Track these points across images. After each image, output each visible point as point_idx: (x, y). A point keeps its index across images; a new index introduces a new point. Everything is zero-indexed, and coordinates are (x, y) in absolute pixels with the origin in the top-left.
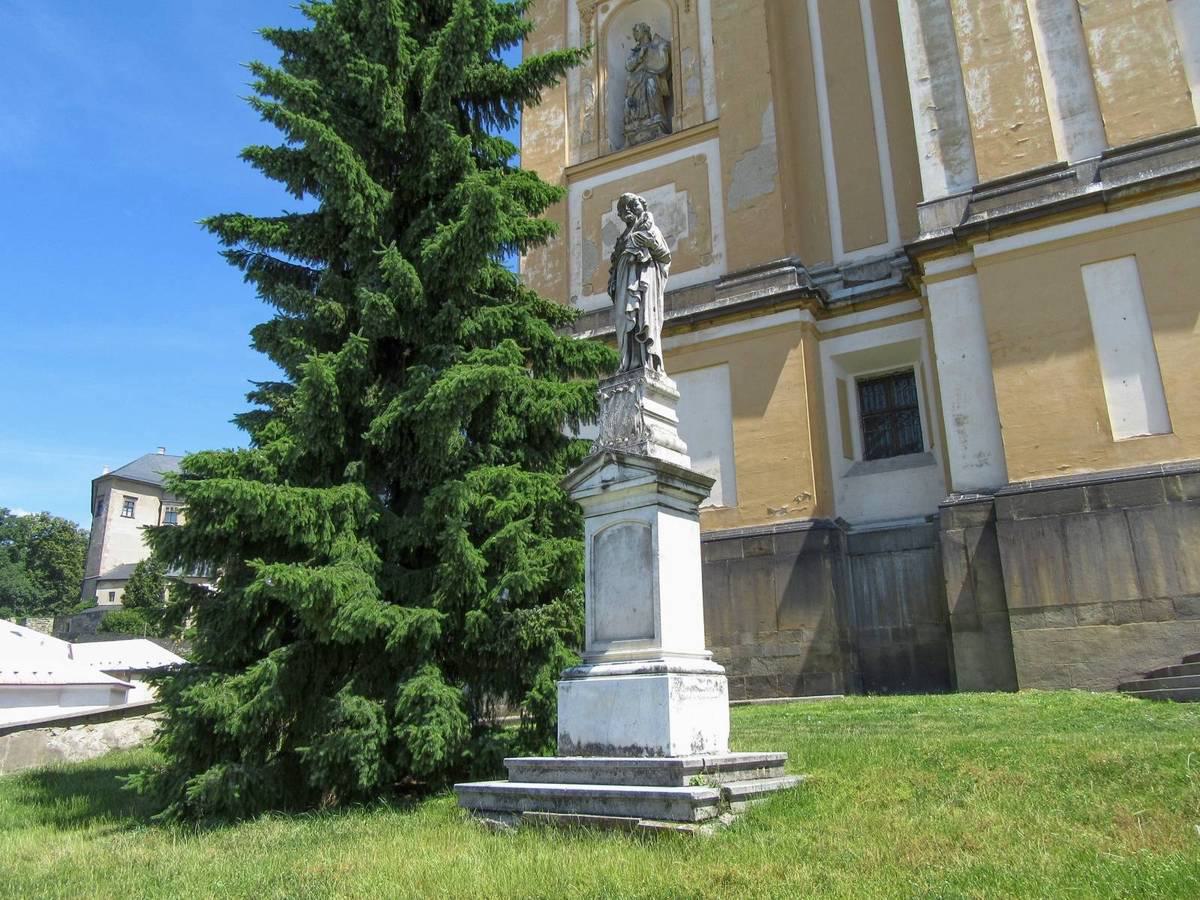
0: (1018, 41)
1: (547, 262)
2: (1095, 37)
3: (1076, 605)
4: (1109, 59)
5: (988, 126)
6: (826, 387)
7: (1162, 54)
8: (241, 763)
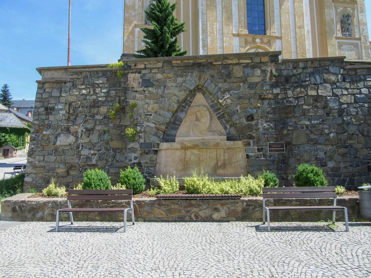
0: (215, 35)
1: (161, 14)
2: (224, 38)
3: (182, 148)
4: (226, 42)
5: (210, 46)
6: (92, 210)
7: (231, 44)
8: (248, 209)
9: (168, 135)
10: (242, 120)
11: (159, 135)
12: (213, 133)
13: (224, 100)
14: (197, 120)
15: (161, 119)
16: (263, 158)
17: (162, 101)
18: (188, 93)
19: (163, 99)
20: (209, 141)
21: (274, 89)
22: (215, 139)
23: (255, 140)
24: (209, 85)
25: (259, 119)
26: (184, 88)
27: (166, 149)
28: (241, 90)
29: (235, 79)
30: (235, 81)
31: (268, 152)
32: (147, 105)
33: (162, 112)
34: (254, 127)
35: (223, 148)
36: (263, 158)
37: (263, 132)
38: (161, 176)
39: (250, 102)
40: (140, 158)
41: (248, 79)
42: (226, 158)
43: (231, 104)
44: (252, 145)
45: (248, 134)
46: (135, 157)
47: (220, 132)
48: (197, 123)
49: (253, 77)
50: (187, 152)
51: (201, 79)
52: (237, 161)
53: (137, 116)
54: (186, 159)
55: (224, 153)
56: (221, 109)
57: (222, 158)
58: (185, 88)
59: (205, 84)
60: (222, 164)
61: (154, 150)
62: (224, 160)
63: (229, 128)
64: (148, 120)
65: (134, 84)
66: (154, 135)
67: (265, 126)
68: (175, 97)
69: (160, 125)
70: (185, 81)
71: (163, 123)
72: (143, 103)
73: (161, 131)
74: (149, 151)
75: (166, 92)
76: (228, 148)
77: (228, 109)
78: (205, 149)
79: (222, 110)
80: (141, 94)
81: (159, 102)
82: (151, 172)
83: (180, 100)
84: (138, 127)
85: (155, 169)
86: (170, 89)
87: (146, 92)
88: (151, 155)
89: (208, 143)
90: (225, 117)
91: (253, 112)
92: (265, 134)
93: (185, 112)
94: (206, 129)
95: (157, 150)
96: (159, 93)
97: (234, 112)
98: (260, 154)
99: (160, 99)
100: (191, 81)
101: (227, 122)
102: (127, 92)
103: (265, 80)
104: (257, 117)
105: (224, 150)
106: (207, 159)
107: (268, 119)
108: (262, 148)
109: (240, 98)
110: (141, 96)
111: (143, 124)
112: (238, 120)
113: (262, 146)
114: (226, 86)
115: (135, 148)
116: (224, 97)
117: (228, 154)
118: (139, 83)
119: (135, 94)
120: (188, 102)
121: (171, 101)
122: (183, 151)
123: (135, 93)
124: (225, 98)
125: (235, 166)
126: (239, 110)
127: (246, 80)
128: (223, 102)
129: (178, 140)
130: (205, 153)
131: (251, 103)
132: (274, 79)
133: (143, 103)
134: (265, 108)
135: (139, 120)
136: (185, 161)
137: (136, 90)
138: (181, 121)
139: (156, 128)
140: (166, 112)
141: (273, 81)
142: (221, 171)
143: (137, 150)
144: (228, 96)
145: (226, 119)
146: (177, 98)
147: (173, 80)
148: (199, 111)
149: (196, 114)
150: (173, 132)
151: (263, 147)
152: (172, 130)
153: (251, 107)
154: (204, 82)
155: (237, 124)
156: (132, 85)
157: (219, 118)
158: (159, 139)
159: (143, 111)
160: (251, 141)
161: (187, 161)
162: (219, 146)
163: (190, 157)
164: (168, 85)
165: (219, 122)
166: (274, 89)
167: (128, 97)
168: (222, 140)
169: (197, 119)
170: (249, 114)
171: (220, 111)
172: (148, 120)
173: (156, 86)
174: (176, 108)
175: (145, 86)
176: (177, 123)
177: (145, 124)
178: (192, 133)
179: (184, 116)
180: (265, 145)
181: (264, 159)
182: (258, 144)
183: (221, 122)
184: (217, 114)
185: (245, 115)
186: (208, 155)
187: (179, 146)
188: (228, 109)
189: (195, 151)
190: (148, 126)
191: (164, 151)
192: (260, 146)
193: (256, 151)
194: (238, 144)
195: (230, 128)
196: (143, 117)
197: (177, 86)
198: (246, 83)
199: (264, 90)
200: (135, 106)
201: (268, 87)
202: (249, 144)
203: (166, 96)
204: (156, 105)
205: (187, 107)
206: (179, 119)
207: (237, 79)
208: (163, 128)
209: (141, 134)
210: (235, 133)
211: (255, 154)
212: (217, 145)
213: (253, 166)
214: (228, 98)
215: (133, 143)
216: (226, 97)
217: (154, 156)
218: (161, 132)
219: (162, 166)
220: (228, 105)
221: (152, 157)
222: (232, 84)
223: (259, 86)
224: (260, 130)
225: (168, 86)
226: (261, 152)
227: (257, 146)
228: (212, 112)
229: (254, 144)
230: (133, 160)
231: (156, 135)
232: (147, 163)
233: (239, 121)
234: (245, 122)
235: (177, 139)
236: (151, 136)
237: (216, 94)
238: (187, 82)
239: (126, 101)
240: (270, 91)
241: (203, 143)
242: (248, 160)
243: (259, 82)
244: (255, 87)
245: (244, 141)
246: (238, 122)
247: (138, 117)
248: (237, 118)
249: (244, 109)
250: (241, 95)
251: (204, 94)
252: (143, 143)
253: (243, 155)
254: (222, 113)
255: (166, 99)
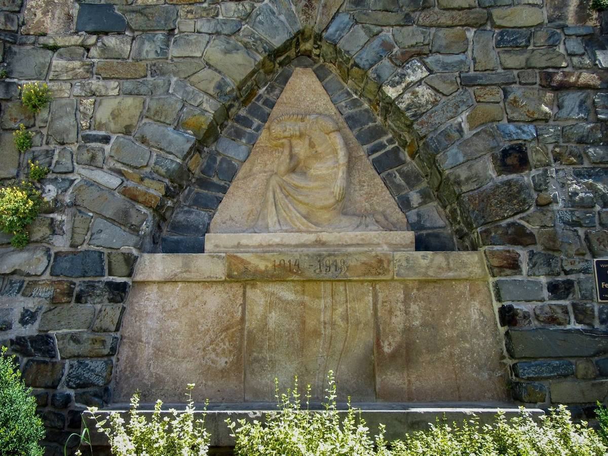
3: (231, 278)
9: (176, 228)
10: (478, 166)
11: (134, 220)
12: (356, 220)
13: (405, 89)
14: (293, 170)
15: (146, 156)
16: (574, 325)
17: (155, 86)
18: (260, 58)
19: (160, 81)
20: (344, 250)
21: (598, 52)
22: (369, 245)
23: (538, 248)
24: (343, 30)
25: (549, 165)
26: (246, 40)
27: (165, 282)
28: (469, 53)
29: (447, 13)
30: (445, 18)
31: (592, 300)
32: (92, 100)
33: (151, 129)
34: (530, 196)
35: (402, 282)
36: (574, 325)
37: (568, 217)
38: (135, 401)
39: (511, 97)
40: (50, 315)
41: (496, 12)
42: (417, 323)
43: (435, 103)
44: (525, 267)
45: (509, 225)
46: (27, 311)
47: (387, 219)
48: (295, 179)
49: (512, 8)
50: (250, 293)
51: (313, 8)
52: (462, 336)
53: (47, 143)
54: (247, 324)
55: (407, 300)
56: (386, 133)
57: (398, 321)
58: (251, 41)
59: (327, 28)
60: (400, 346)
61: (109, 284)
62: (408, 330)
63: (420, 204)
64: (93, 158)
65: (48, 20)
66: (112, 221)
67: (575, 194)
68: (206, 73)
69: (142, 180)
70: (249, 15)
71: (157, 172)
72: (77, 91)
73: (146, 204)
74: (92, 286)
75: (174, 51)
76: (420, 281)
77: (422, 124)
78: (328, 285)
79: (390, 136)
80: (72, 59)
81: (143, 89)
82: (94, 378)
83: (228, 85)
84: (50, 187)
85: (110, 366)
86: (188, 43)
87: (94, 52)
88: (99, 306)
89: (339, 259)
90: (403, 163)
91: (524, 136)
92: (577, 224)
93: (249, 142)
94: (332, 201)
95: (125, 284)
96: (144, 53)
97: (446, 134)
98: (558, 306)
99: (149, 78)
100: (274, 13)
101: (411, 179)
102: (15, 48)
103: (559, 18)
104: (540, 157)
105: (406, 287)
106: (333, 324)
107: (586, 164)
108: (570, 283)
109: (467, 82)
110: (71, 65)
111: (71, 177)
112: (464, 167)
113: (567, 273)
114: (411, 36)
115: (28, 275)
116: (403, 76)
117: (422, 304)
118: (69, 17)
119: (43, 57)
120: (260, 103)
121: (190, 88)
122: (237, 289)
123: (50, 53)
124: (409, 79)
125: (451, 355)
126: (465, 126)
127: (490, 17)
128: (400, 96)
129: (217, 246)
130: (329, 300)
131: (515, 101)
132: (595, 15)
133: (77, 91)
134: (570, 123)
135: (56, 158)
136: (243, 329)
137: (51, 42)
138: (231, 173)
139: (125, 192)
140: (171, 128)
141: (591, 23)
142: (393, 379)
143: (35, 283)
144: (421, 73)
145: (405, 168)
146: (218, 78)
147: (205, 9)
148: (301, 136)
149: (291, 147)
150: (198, 216)
151: (572, 277)
152: (194, 209)
153: (515, 116)
154: (326, 20)
155: (458, 183)
156: (41, 23)
157: (380, 166)
158: (134, 239)
159: (72, 121)
160: (523, 254)
161: (250, 332)
162: (386, 271)
163: (265, 318)
164: (183, 28)
165: (378, 180)
166: (598, 52)
167: (18, 67)
168: (396, 247)
169: (295, 168)
170: (507, 145)
171: (384, 140)
172: (93, 158)
173: (133, 31)
174: (210, 116)
175: (89, 29)
176: (215, 180)
177: (82, 173)
178: (272, 219)
179: (242, 157)
180: (579, 271)
181: (579, 327)
182: (549, 265)
183: (388, 182)
184: (373, 151)
185: (493, 148)
186: (340, 310)
187: (219, 270)
188: (422, 124)
189: (286, 293)
190: (91, 183)
191: (155, 288)
192: (558, 274)
193: (546, 294)
194: (464, 265)
195: (423, 203)
196: (74, 148)
197: (218, 33)
198: (489, 28)
199: (560, 55)
200: (41, 101)
201: (575, 45)
202: (514, 266)
203: (171, 67)
204: (129, 101)
205: (256, 122)
206: (224, 165)
207: (454, 13)
208: (152, 191)
209: (58, 217)
210: (441, 223)
211: (542, 308)
212: (379, 266)
213: (535, 358)
214: (419, 82)
215: (21, 250)
216: (412, 78)
217: (108, 308)
218: (144, 210)
219: (148, 351)
220: (420, 106)
221: (97, 315)
222: (433, 30)
223: (541, 38)
224: (555, 207)
225: (180, 32)
226: (565, 298)
227: (547, 275)
228: (354, 142)
229: (533, 266)
230: (16, 325)
231: (122, 220)
232: (75, 339)
233: (470, 168)
234: (494, 176)
235: (211, 241)
236: (100, 223)
237: (371, 66)
238: (260, 17)
239: (9, 84)
240: (586, 58)
241: (319, 257)
242: (511, 333)
243: (540, 25)
244: (523, 42)
245: (493, 253)
246: (463, 174)
247: (52, 147)
248: (461, 159)
249: (481, 123)
250: (472, 73)
251: (321, 74)
252: (67, 254)
253: (485, 309)
254: (390, 147)
255: (174, 80)
